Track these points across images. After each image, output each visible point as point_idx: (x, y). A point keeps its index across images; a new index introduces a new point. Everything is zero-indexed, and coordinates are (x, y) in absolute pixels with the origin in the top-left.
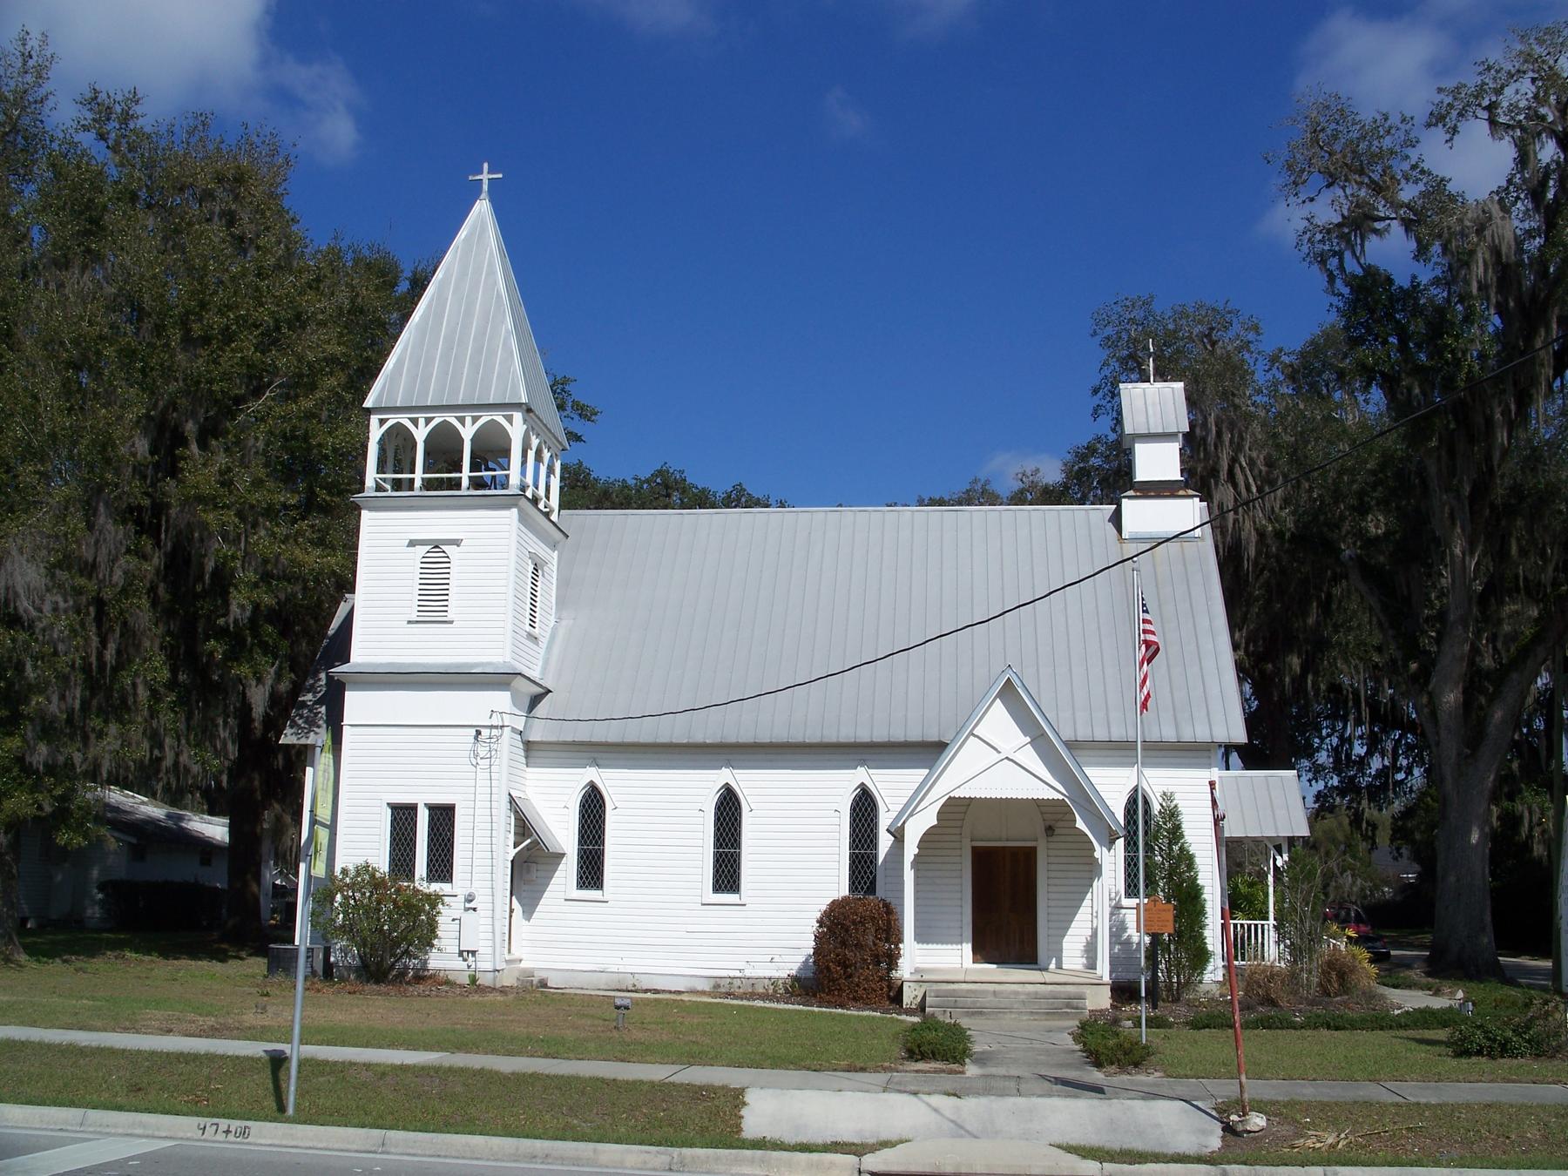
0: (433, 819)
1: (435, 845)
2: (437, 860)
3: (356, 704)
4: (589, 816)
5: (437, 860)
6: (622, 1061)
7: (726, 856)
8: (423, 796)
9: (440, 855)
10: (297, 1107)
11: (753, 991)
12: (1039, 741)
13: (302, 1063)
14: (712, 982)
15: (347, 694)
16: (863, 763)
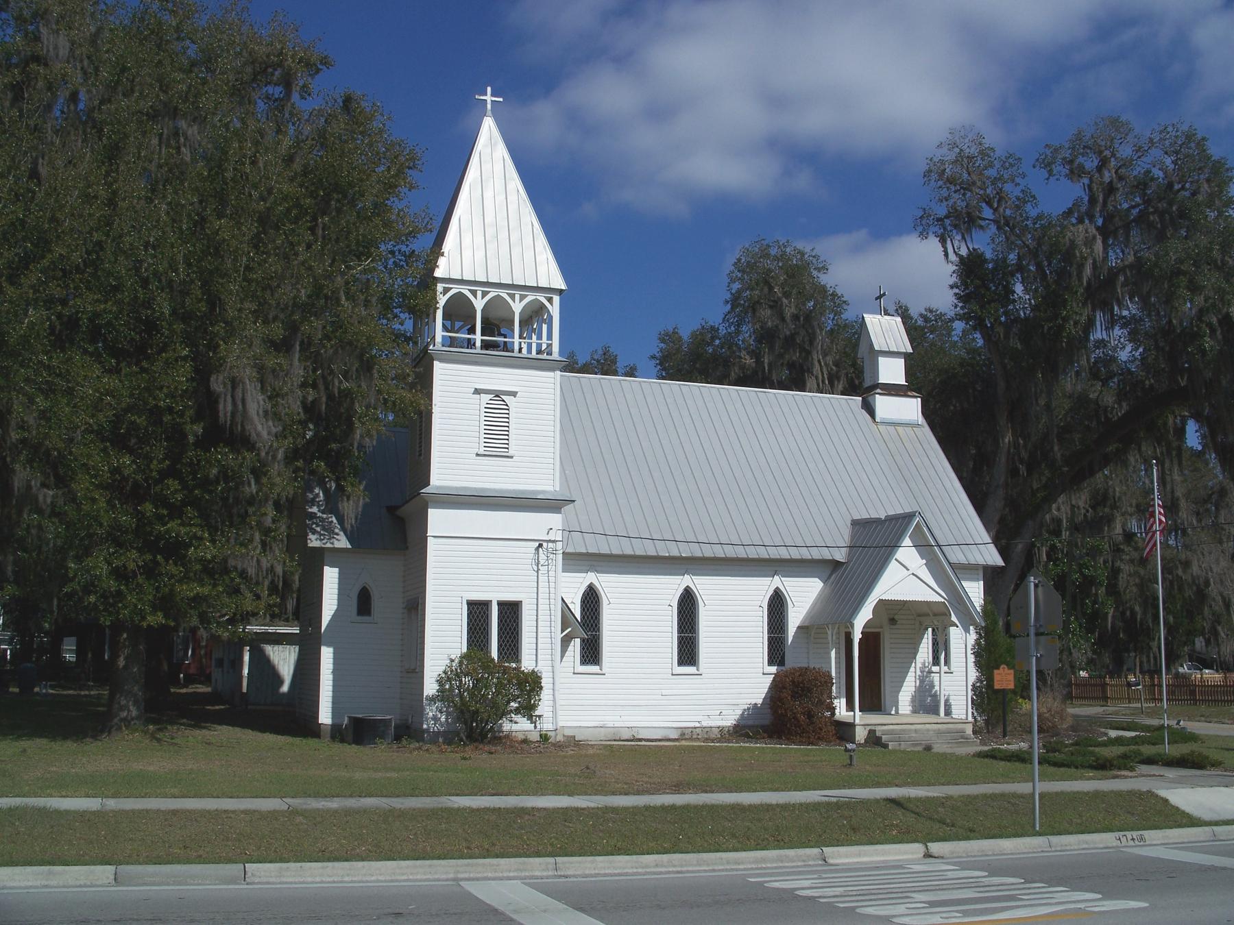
0: (501, 613)
1: (503, 633)
2: (506, 645)
3: (438, 520)
4: (588, 610)
5: (506, 645)
6: (626, 794)
7: (686, 639)
8: (494, 595)
9: (508, 641)
10: (1041, 826)
11: (705, 735)
12: (934, 565)
13: (1042, 796)
14: (679, 732)
15: (429, 510)
16: (686, 572)
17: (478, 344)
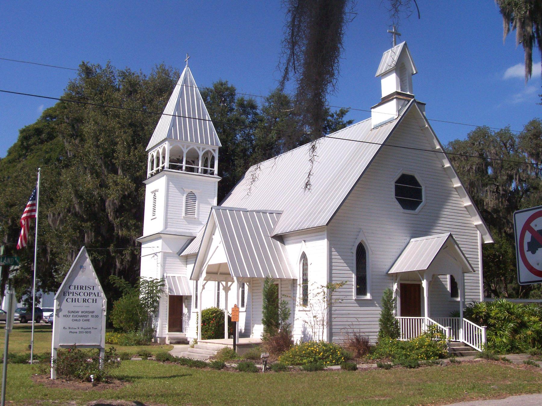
17: (184, 168)
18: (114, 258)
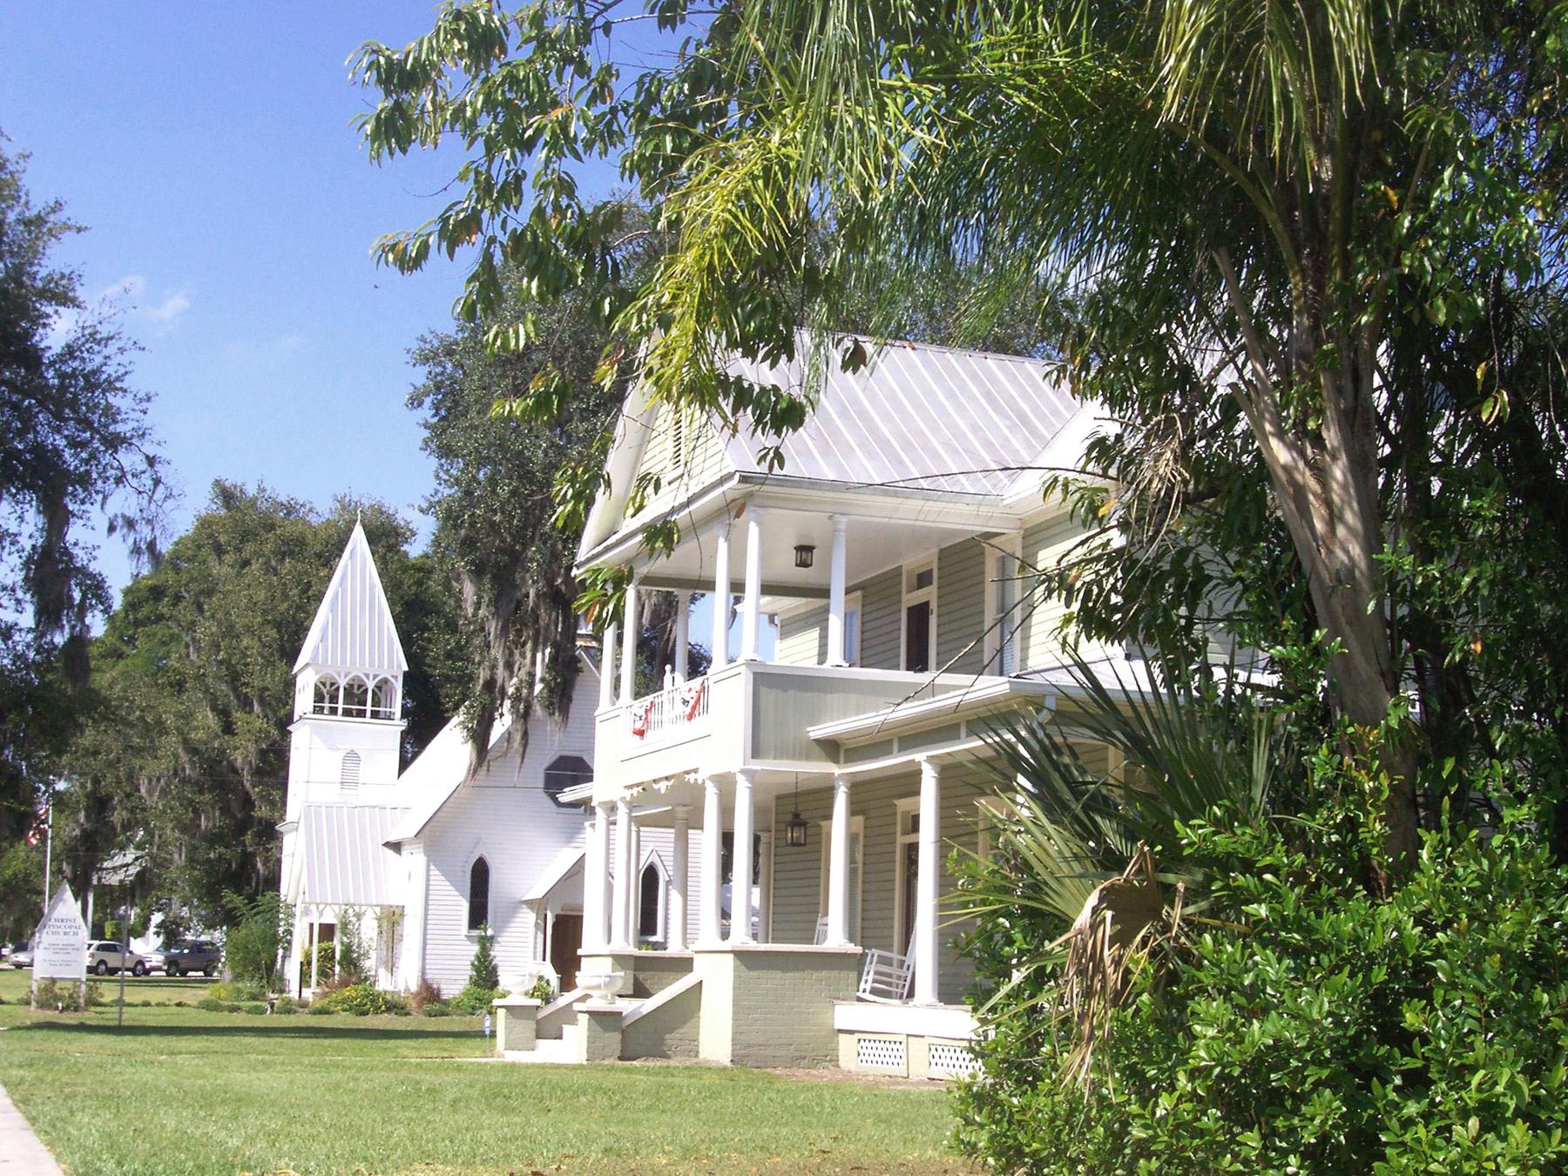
17: (340, 711)
18: (253, 855)
